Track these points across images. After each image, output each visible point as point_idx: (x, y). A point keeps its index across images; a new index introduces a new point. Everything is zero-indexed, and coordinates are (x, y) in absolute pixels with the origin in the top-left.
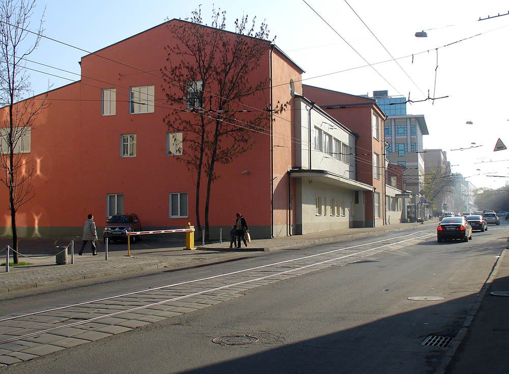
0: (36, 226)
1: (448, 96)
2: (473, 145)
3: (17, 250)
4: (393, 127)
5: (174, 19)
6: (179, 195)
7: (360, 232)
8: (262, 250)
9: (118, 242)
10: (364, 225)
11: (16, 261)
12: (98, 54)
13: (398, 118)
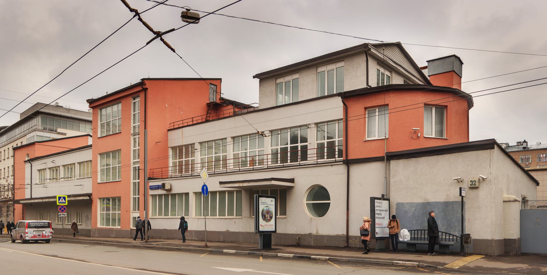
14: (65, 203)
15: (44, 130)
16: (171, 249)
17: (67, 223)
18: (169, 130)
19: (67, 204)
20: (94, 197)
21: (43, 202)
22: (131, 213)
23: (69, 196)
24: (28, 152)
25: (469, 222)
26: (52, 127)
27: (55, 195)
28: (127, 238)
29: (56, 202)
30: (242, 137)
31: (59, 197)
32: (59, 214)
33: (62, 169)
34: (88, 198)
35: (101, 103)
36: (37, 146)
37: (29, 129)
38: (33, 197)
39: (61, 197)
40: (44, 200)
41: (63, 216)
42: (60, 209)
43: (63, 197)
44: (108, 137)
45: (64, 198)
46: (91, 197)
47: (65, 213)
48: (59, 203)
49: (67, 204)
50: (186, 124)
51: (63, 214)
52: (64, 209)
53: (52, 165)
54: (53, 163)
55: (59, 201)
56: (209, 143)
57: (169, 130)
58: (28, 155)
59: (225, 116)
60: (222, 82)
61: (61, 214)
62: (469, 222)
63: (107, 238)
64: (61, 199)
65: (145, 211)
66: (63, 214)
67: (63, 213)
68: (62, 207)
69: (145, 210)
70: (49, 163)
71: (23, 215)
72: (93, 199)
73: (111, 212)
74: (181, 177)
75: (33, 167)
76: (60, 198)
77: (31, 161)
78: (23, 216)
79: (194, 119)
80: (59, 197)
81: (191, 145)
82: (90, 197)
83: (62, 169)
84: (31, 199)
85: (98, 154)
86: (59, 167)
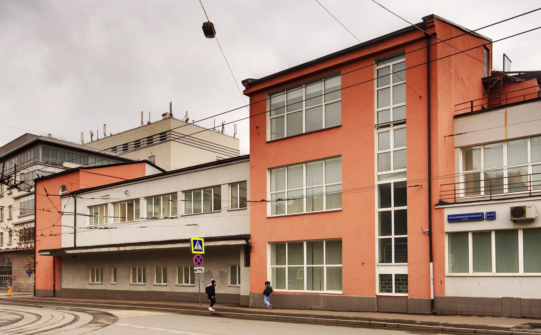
0: (153, 201)
1: (142, 112)
2: (165, 117)
3: (284, 114)
4: (30, 169)
5: (27, 133)
6: (142, 268)
7: (88, 310)
8: (8, 249)
9: (199, 273)
10: (191, 194)
11: (499, 98)
12: (285, 246)
13: (358, 325)
14: (202, 251)
15: (46, 164)
16: (455, 331)
17: (155, 283)
18: (456, 117)
19: (203, 252)
20: (255, 240)
21: (126, 251)
22: (377, 268)
23: (207, 240)
24: (65, 183)
25: (520, 283)
26: (54, 160)
27: (188, 238)
28: (58, 297)
29: (189, 249)
30: (121, 203)
31: (194, 241)
32: (195, 268)
33: (143, 204)
34: (243, 242)
35: (306, 73)
36: (82, 174)
37: (12, 168)
38: (78, 245)
39: (197, 241)
40: (122, 249)
41: (200, 272)
42: (196, 260)
43: (199, 241)
44: (310, 136)
45: (200, 242)
46: (250, 241)
47: (202, 266)
48: (195, 250)
49: (203, 252)
50: (522, 99)
51: (200, 269)
52: (201, 260)
53: (123, 197)
54: (126, 194)
55: (194, 248)
56: (164, 196)
57: (456, 117)
58: (64, 188)
59: (510, 102)
60: (493, 46)
61: (198, 268)
62: (520, 283)
63: (292, 310)
64: (197, 244)
65: (431, 264)
66: (200, 269)
67: (200, 268)
68: (198, 257)
69: (431, 260)
70: (96, 198)
71: (54, 271)
72: (253, 245)
73: (287, 266)
74: (530, 196)
75: (77, 204)
76: (195, 242)
77: (75, 194)
78: (54, 273)
79: (475, 104)
80: (194, 241)
81: (463, 148)
82: (247, 241)
83: (143, 204)
84: (75, 248)
85: (267, 169)
86: (137, 200)
